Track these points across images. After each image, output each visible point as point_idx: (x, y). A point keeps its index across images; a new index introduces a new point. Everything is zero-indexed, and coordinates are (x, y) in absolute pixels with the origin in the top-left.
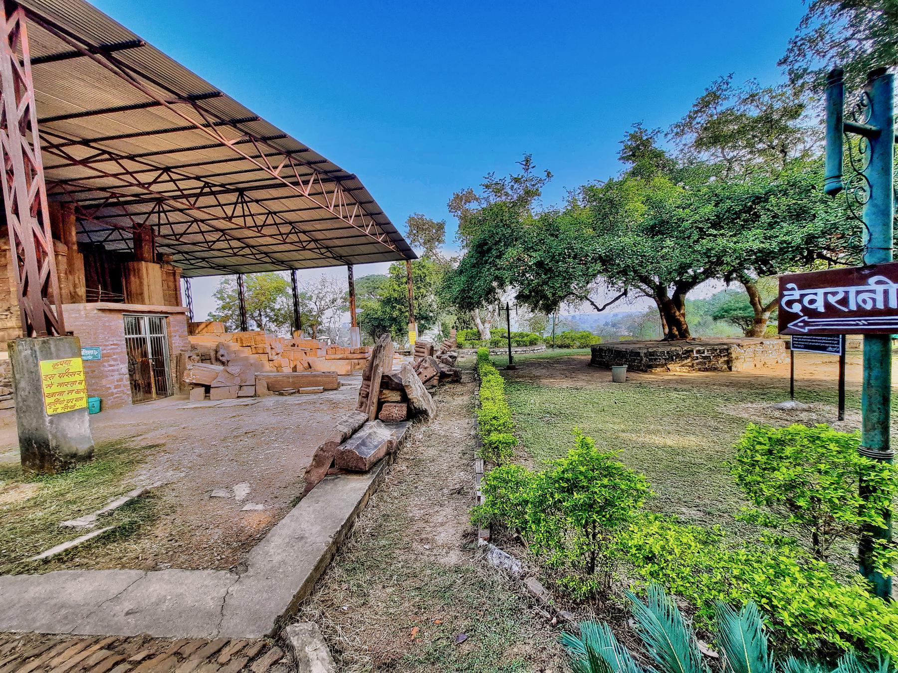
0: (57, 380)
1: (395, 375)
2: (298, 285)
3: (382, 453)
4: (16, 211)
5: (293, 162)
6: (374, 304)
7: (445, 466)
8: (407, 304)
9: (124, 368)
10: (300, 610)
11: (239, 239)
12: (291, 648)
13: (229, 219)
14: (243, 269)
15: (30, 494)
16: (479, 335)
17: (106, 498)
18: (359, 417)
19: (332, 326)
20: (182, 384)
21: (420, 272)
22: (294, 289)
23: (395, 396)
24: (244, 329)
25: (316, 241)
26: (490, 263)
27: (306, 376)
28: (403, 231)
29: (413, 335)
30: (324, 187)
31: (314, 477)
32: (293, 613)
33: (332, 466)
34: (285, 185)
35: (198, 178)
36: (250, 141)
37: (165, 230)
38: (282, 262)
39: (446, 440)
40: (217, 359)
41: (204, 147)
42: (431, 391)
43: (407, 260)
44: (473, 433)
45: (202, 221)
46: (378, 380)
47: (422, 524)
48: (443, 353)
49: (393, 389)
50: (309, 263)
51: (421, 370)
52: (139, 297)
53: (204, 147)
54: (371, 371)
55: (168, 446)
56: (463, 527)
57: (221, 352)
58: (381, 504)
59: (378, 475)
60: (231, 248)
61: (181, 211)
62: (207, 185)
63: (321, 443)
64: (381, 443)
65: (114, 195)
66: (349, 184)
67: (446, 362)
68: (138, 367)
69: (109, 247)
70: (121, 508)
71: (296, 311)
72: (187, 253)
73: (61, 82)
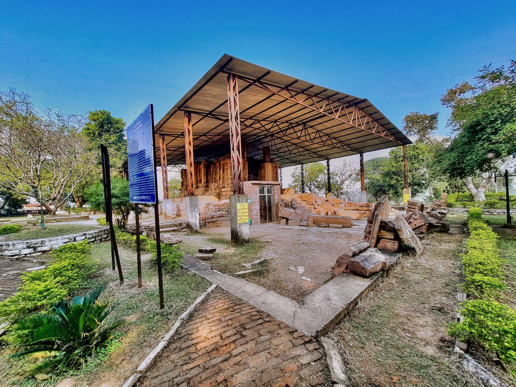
0: (241, 211)
1: (390, 222)
2: (331, 168)
3: (379, 268)
4: (233, 150)
5: (330, 102)
6: (377, 176)
7: (428, 289)
8: (403, 175)
9: (258, 208)
10: (327, 334)
11: (302, 147)
12: (323, 347)
13: (299, 138)
14: (303, 162)
15: (233, 252)
16: (471, 198)
17: (253, 259)
18: (364, 244)
19: (349, 190)
20: (277, 217)
21: (414, 153)
22: (328, 170)
23: (390, 236)
24: (303, 192)
25: (341, 142)
26: (484, 139)
27: (333, 218)
28: (400, 125)
29: (407, 196)
30: (347, 111)
31: (336, 272)
32: (325, 331)
33: (346, 268)
34: (325, 115)
35: (287, 122)
36: (310, 98)
37: (274, 148)
38: (323, 156)
39: (431, 273)
40: (292, 206)
41: (290, 107)
42: (419, 236)
43: (403, 146)
44: (458, 271)
45: (288, 141)
46: (377, 225)
47: (405, 320)
48: (433, 210)
49: (388, 231)
50: (337, 155)
51: (411, 220)
52: (263, 178)
53: (290, 107)
54: (373, 217)
55: (273, 243)
56: (441, 335)
57: (293, 203)
58: (376, 298)
59: (375, 281)
60: (299, 152)
61: (280, 138)
62: (291, 124)
63: (341, 255)
64: (378, 262)
65: (258, 136)
66: (363, 105)
67: (435, 217)
68: (263, 207)
69: (255, 158)
70: (258, 264)
71: (329, 182)
72: (281, 157)
73: (245, 98)
